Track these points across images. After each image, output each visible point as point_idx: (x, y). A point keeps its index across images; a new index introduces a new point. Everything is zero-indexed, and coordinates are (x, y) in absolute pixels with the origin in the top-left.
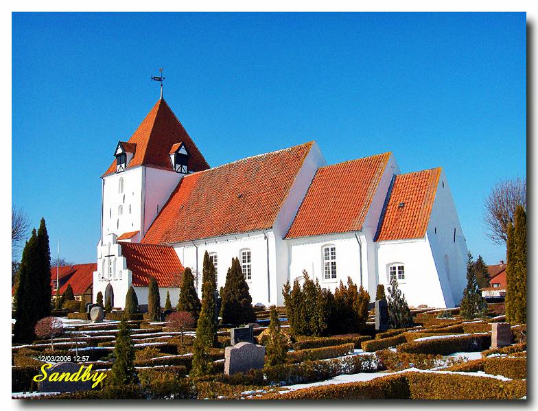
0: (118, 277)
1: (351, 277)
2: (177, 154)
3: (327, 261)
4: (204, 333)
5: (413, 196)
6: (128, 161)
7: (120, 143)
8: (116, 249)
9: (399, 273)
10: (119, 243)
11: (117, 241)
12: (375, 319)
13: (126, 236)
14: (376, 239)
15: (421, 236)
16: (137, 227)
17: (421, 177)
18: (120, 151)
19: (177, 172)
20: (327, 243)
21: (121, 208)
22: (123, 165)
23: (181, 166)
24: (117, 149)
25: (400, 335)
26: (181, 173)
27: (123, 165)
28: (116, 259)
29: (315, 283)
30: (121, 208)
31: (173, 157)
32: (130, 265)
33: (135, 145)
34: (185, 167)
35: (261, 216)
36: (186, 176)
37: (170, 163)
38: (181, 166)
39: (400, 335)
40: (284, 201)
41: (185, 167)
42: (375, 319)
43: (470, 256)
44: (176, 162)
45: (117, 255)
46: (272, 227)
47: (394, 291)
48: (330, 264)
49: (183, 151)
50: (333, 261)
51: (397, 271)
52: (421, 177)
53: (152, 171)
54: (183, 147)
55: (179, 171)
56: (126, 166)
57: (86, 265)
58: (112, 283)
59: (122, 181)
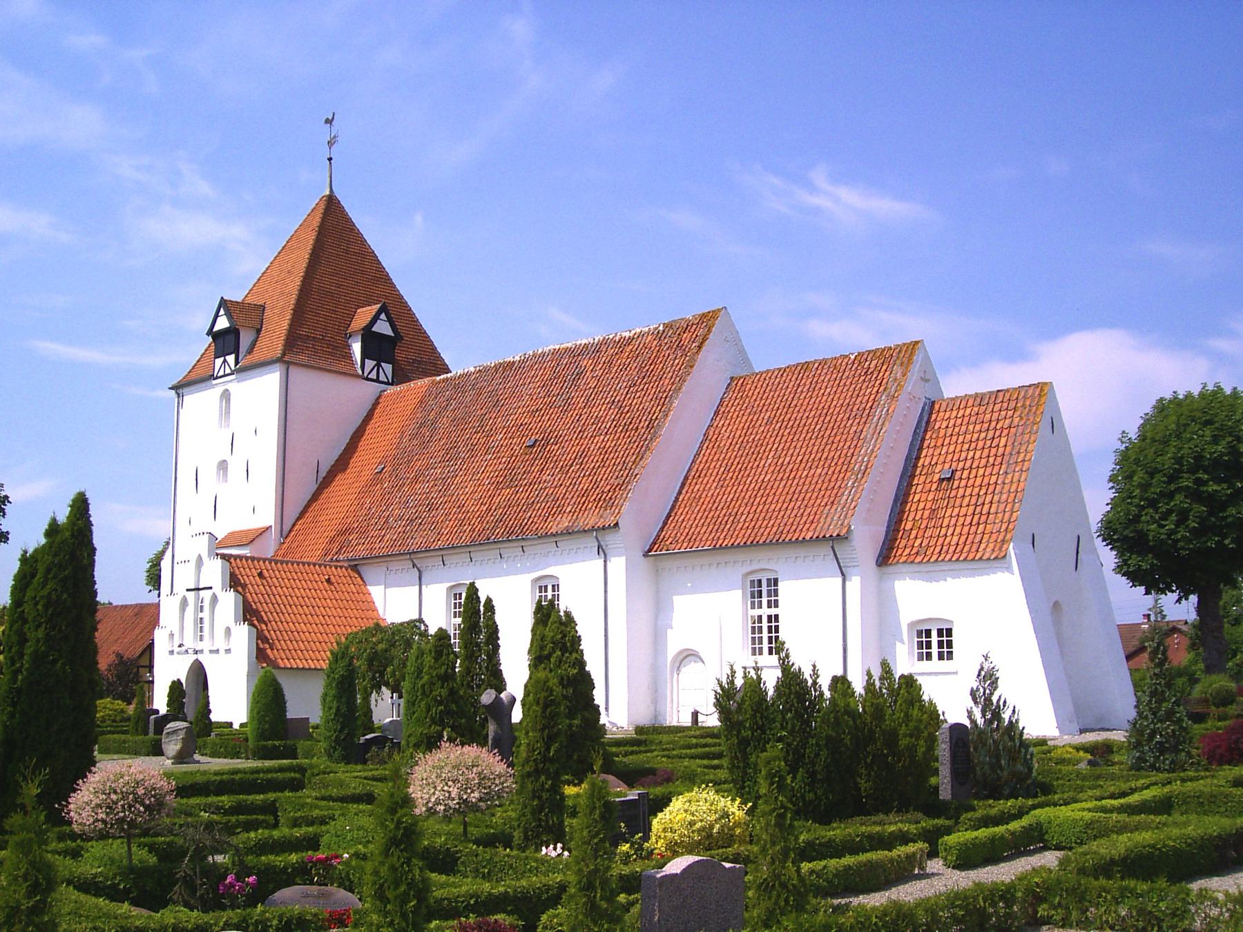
0: (220, 643)
1: (997, 661)
2: (368, 336)
3: (757, 612)
4: (524, 815)
5: (978, 454)
6: (243, 349)
7: (223, 303)
8: (214, 572)
9: (940, 644)
10: (223, 557)
11: (218, 547)
12: (943, 780)
13: (236, 539)
14: (885, 558)
15: (1000, 558)
16: (266, 516)
17: (997, 407)
18: (223, 323)
19: (367, 379)
20: (756, 566)
21: (223, 466)
22: (231, 359)
23: (378, 365)
24: (217, 316)
25: (1025, 821)
26: (377, 380)
27: (231, 359)
28: (214, 599)
29: (810, 682)
30: (223, 466)
31: (357, 348)
32: (249, 613)
33: (263, 308)
34: (388, 368)
35: (586, 493)
36: (391, 390)
37: (349, 356)
38: (378, 365)
39: (1025, 821)
40: (649, 459)
41: (388, 368)
42: (943, 780)
43: (150, 591)
44: (365, 355)
45: (217, 588)
46: (617, 524)
47: (988, 700)
48: (765, 620)
49: (383, 327)
50: (773, 611)
51: (934, 639)
52: (997, 407)
53: (304, 379)
54: (383, 316)
55: (373, 375)
56: (237, 362)
57: (126, 606)
58: (205, 659)
59: (226, 395)
